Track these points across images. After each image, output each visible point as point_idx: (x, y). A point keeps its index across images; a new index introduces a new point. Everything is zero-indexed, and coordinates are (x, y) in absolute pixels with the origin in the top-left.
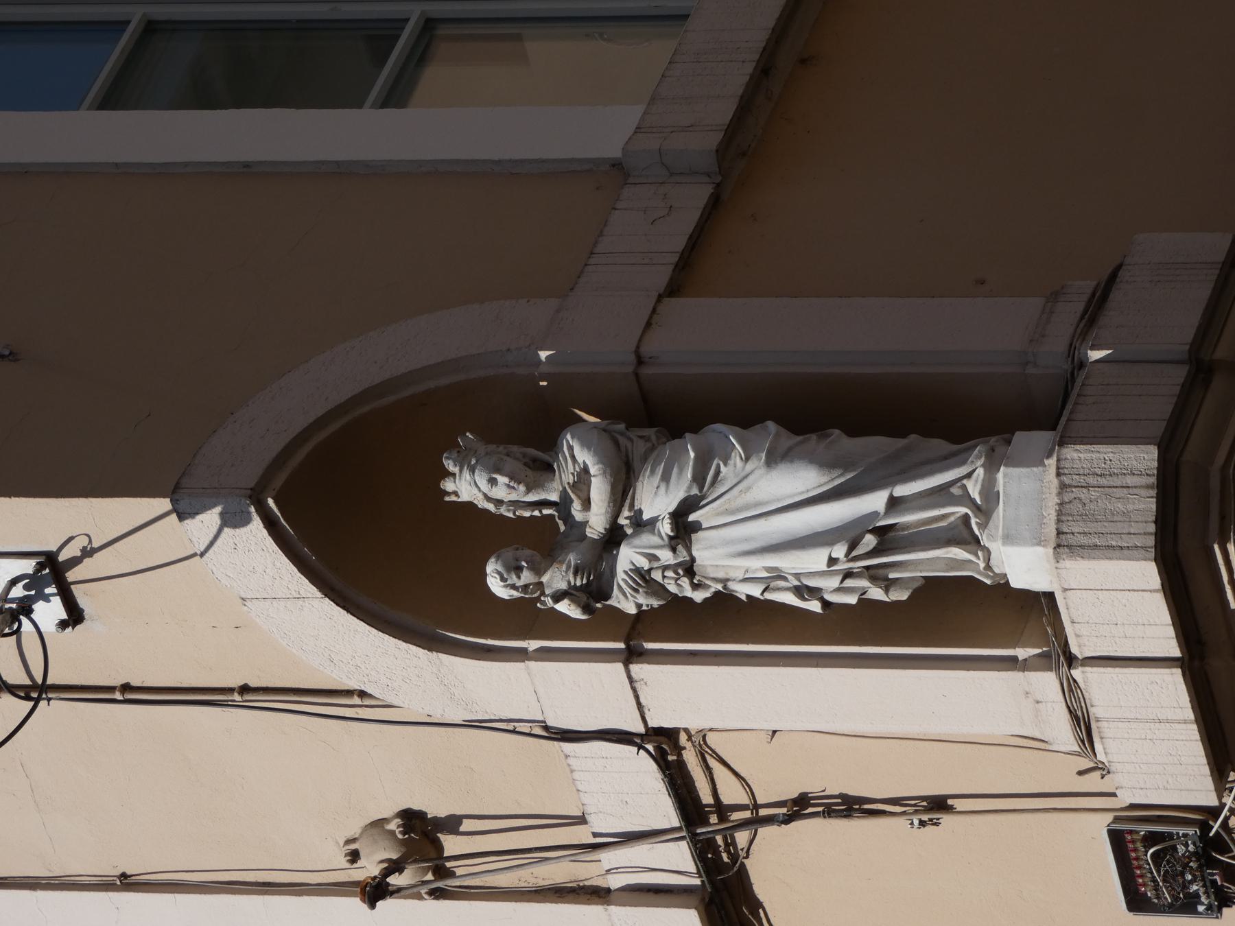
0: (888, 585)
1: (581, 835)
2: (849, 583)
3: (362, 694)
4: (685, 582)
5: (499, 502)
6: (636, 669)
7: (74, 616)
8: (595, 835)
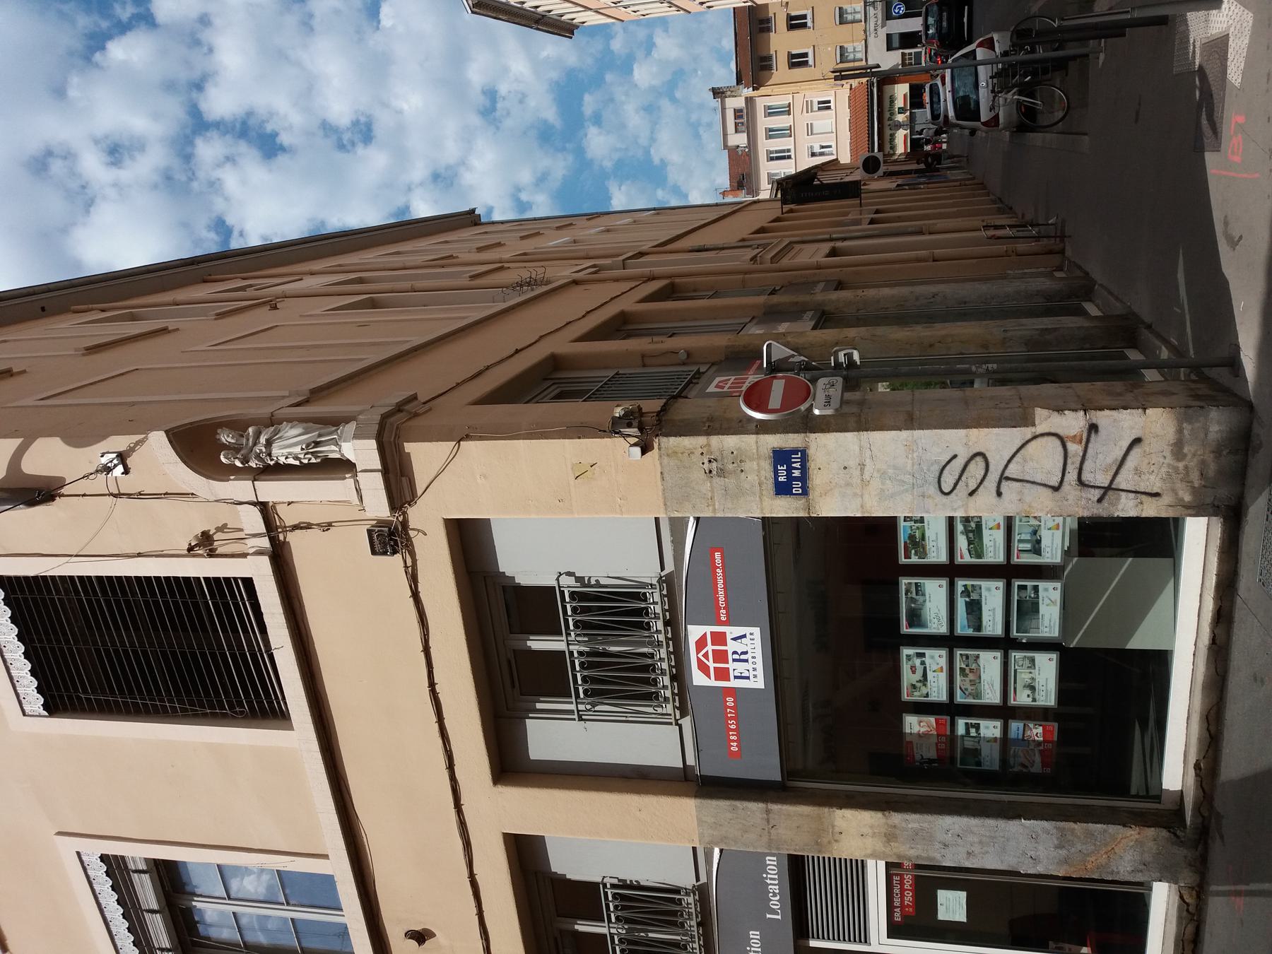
0: (316, 457)
1: (241, 535)
2: (306, 456)
3: (193, 494)
4: (268, 458)
5: (229, 442)
6: (255, 482)
7: (126, 472)
8: (246, 535)
